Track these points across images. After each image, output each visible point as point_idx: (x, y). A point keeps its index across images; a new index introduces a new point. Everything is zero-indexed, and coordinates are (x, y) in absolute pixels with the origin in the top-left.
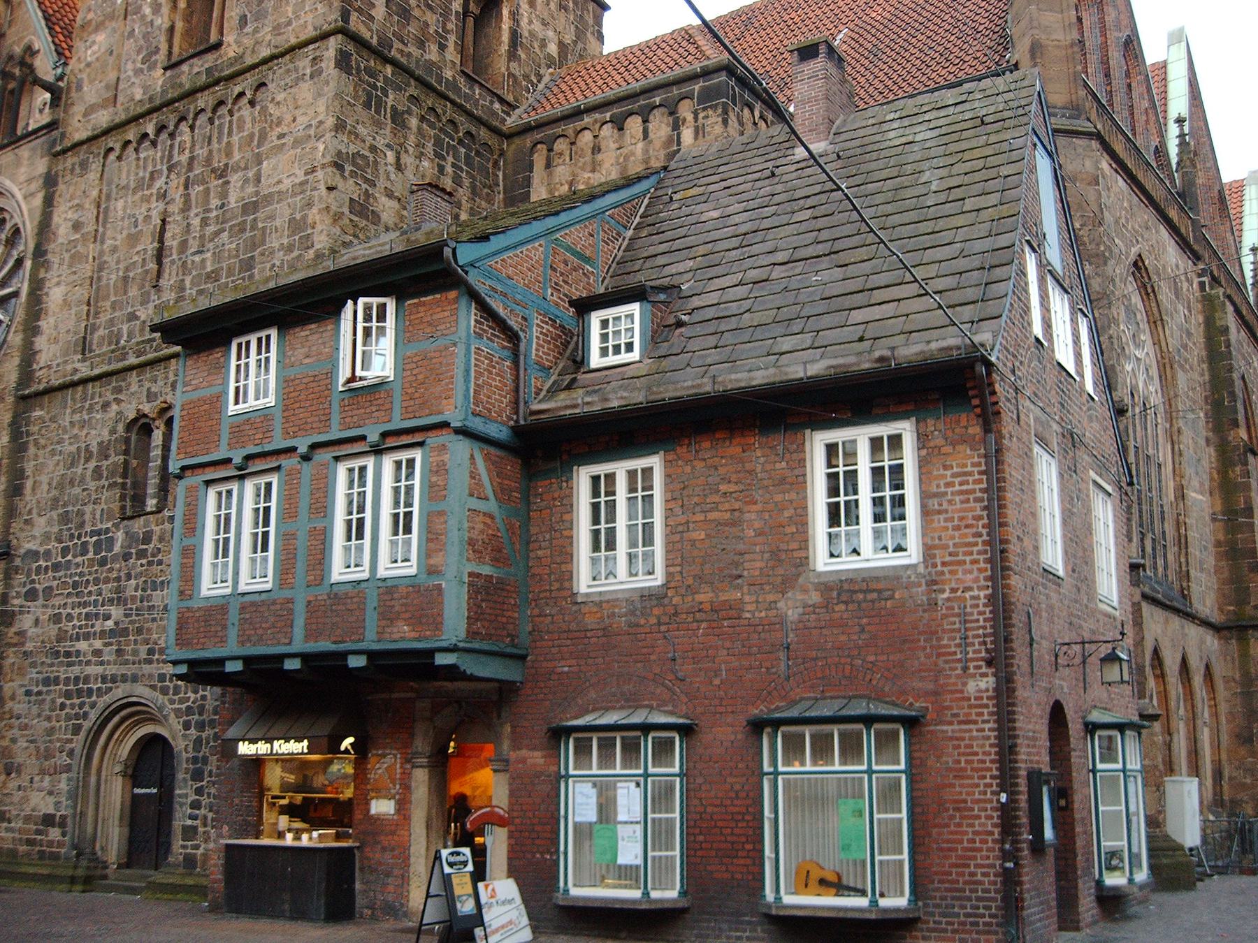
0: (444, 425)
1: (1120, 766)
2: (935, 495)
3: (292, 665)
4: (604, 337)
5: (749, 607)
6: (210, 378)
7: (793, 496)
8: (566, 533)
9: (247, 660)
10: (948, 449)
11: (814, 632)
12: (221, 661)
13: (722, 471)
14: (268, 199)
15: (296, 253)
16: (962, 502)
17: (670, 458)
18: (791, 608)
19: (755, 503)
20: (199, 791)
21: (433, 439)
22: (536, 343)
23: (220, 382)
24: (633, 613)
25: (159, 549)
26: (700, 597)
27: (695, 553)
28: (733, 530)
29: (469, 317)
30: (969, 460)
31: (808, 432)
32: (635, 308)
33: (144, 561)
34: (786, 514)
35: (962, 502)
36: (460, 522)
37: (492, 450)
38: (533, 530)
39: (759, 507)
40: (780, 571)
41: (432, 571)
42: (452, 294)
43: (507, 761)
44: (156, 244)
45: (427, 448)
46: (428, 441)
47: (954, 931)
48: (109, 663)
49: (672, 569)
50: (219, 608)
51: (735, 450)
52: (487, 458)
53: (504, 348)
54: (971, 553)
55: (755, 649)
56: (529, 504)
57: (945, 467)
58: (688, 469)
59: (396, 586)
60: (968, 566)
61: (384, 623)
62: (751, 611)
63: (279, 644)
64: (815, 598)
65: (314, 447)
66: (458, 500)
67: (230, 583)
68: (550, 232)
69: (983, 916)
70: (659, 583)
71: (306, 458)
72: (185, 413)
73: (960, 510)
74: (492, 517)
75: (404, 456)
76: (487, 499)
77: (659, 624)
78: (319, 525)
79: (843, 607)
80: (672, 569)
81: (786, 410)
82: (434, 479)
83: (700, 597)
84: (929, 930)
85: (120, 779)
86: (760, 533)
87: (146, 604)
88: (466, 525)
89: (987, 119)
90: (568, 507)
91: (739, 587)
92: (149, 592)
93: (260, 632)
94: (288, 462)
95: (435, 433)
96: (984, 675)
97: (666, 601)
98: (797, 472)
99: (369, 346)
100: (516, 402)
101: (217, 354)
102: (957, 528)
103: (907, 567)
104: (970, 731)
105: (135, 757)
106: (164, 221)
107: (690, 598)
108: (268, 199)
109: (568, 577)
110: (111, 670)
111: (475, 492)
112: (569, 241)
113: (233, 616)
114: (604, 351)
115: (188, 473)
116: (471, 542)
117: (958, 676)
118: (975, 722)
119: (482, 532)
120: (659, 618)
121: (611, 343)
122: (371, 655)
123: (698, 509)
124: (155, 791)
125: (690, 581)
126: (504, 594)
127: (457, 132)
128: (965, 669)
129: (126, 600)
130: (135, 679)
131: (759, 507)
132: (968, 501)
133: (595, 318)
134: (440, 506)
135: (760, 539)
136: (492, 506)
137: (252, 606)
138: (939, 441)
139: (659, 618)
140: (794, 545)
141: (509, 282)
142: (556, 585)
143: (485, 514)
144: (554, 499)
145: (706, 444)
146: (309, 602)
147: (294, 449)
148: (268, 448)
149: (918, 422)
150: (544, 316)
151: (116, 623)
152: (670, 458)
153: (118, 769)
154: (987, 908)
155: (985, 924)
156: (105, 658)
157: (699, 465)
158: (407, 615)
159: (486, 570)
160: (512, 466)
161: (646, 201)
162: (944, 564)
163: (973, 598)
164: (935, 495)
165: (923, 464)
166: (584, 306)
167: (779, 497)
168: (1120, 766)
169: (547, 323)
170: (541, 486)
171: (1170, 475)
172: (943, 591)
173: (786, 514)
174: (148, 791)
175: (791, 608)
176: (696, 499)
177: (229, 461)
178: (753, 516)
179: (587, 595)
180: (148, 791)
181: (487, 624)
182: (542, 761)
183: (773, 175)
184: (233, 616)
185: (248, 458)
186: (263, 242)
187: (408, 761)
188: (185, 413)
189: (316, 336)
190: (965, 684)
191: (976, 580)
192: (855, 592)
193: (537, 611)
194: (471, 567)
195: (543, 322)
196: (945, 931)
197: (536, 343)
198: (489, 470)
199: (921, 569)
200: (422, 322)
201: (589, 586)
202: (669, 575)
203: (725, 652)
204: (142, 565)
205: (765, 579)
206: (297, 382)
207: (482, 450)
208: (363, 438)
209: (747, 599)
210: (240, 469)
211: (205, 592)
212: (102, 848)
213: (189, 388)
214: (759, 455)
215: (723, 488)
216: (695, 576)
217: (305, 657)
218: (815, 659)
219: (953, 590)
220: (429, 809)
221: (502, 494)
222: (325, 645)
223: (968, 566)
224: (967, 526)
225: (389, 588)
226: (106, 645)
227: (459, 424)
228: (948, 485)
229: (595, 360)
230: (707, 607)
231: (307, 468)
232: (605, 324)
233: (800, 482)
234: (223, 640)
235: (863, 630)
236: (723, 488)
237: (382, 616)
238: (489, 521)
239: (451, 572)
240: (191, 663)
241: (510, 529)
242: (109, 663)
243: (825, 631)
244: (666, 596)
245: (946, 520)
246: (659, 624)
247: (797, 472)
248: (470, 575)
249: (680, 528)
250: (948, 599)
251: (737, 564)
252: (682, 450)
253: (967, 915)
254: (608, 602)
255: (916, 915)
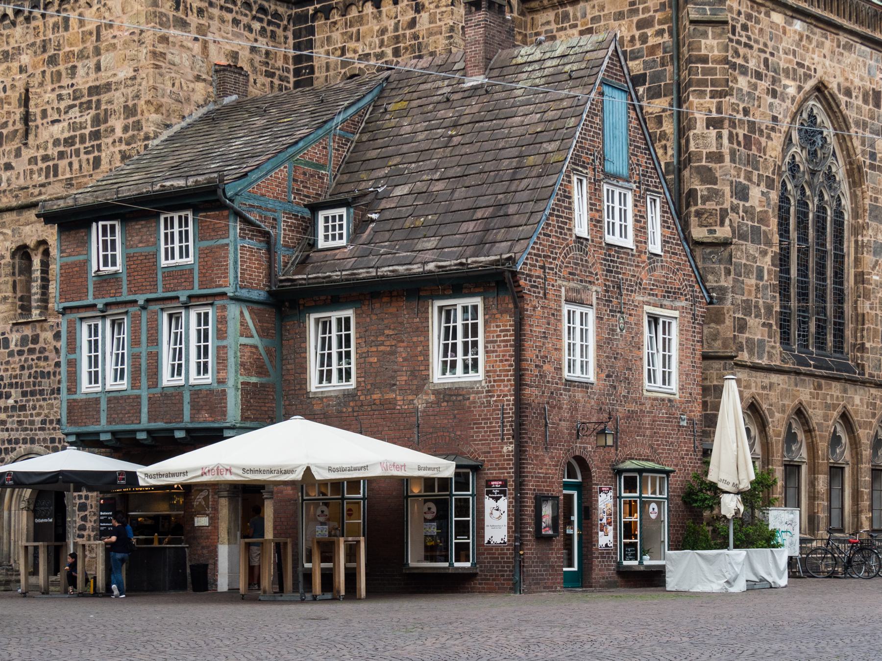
0: (224, 294)
1: (638, 494)
2: (492, 342)
3: (142, 436)
4: (326, 229)
5: (399, 403)
6: (78, 249)
7: (422, 339)
8: (303, 355)
9: (113, 433)
10: (498, 316)
11: (432, 418)
12: (97, 434)
13: (386, 321)
14: (108, 87)
15: (130, 133)
16: (504, 346)
17: (359, 312)
18: (420, 403)
19: (403, 342)
20: (84, 518)
21: (219, 302)
22: (282, 233)
23: (85, 252)
24: (339, 404)
25: (45, 348)
26: (375, 397)
27: (372, 371)
28: (392, 357)
29: (235, 228)
30: (508, 322)
31: (430, 301)
32: (343, 211)
33: (34, 357)
34: (419, 349)
35: (504, 346)
36: (235, 353)
37: (255, 306)
38: (285, 352)
39: (405, 344)
40: (415, 382)
41: (221, 382)
42: (226, 213)
43: (272, 492)
44: (22, 109)
45: (215, 307)
46: (216, 302)
47: (493, 580)
48: (12, 430)
49: (359, 379)
50: (92, 402)
51: (393, 310)
52: (251, 312)
53: (260, 241)
54: (507, 376)
55: (402, 427)
56: (282, 335)
57: (497, 326)
58: (368, 319)
59: (200, 390)
60: (506, 383)
61: (194, 412)
62: (400, 405)
63: (133, 423)
64: (432, 398)
65: (148, 301)
66: (234, 339)
67: (100, 384)
68: (292, 156)
69: (506, 571)
70: (353, 387)
71: (143, 308)
72: (63, 271)
73: (503, 351)
74: (256, 347)
75: (202, 310)
76: (252, 336)
77: (353, 411)
78: (154, 350)
79: (445, 404)
80: (359, 379)
81: (417, 290)
82: (219, 326)
83: (375, 397)
84: (482, 580)
85: (25, 512)
86: (405, 360)
87: (37, 388)
88: (239, 354)
89: (574, 75)
90: (304, 339)
91: (394, 391)
92: (39, 379)
93: (121, 416)
94: (132, 309)
95: (219, 298)
96: (511, 443)
97: (357, 398)
98: (424, 325)
99: (177, 245)
100: (270, 275)
101: (82, 233)
102: (501, 361)
103: (476, 382)
104: (504, 473)
105: (35, 497)
106: (27, 90)
107: (369, 397)
108: (108, 87)
109: (304, 382)
110: (14, 435)
111: (245, 332)
112: (307, 158)
113: (103, 405)
114: (326, 238)
115: (68, 311)
116: (243, 364)
117: (499, 444)
118: (506, 469)
119: (250, 357)
120: (353, 407)
121: (330, 233)
122: (188, 431)
123: (373, 344)
124: (51, 520)
125: (369, 387)
126: (265, 393)
127: (251, 10)
128: (503, 439)
129: (22, 384)
130: (33, 441)
131: (405, 344)
132: (507, 346)
133: (321, 215)
134: (224, 343)
135: (405, 363)
136: (256, 340)
137: (116, 400)
138: (495, 311)
139: (353, 407)
140: (422, 368)
141: (262, 198)
142: (298, 387)
143: (251, 346)
144: (296, 334)
145: (377, 305)
146: (150, 398)
147: (136, 301)
148: (119, 299)
149: (484, 299)
150: (289, 214)
151: (16, 402)
152: (359, 312)
153: (23, 505)
154: (508, 567)
155: (508, 575)
156: (9, 426)
157: (374, 317)
158: (208, 407)
159: (254, 380)
160: (269, 314)
161: (371, 109)
162: (494, 381)
163: (507, 400)
164: (492, 342)
165: (486, 323)
166: (315, 208)
167: (415, 339)
168: (638, 494)
169: (291, 218)
170: (289, 325)
171: (852, 264)
172: (493, 396)
173: (419, 349)
174: (46, 520)
175: (420, 403)
176: (372, 338)
177: (95, 306)
178: (402, 350)
179: (315, 393)
180: (46, 520)
181: (254, 412)
182: (291, 492)
183: (448, 100)
184: (103, 405)
185: (107, 305)
186: (106, 121)
187: (216, 494)
188: (63, 271)
189: (145, 230)
190: (502, 448)
191: (509, 391)
192: (452, 395)
193: (287, 403)
194: (242, 379)
195: (287, 218)
196: (489, 579)
197: (282, 233)
198: (252, 319)
199: (483, 384)
200: (208, 228)
201: (317, 388)
202: (358, 382)
203: (387, 429)
204: (33, 360)
205: (407, 387)
206: (135, 258)
207: (248, 307)
208: (177, 298)
209: (399, 398)
210: (102, 311)
211: (84, 390)
212: (15, 562)
213: (64, 255)
214: (404, 312)
215: (387, 332)
216: (372, 384)
217: (149, 432)
218: (431, 433)
219: (499, 396)
220: (229, 523)
221: (263, 333)
222: (160, 425)
223: (506, 383)
224: (506, 360)
225: (197, 392)
226: (8, 417)
227: (231, 295)
228: (498, 336)
229: (321, 244)
230: (378, 402)
231: (144, 315)
232: (326, 219)
233: (424, 330)
234: (98, 421)
235: (455, 417)
236: (387, 332)
237: (193, 408)
238: (254, 350)
239: (231, 382)
240: (78, 435)
241: (268, 352)
242: (12, 430)
243: (437, 418)
244: (357, 395)
245: (496, 356)
246: (353, 411)
247: (424, 325)
248: (242, 383)
249: (364, 355)
250: (495, 401)
251: (393, 378)
252: (365, 308)
253: (499, 571)
254: (326, 397)
255: (475, 571)
